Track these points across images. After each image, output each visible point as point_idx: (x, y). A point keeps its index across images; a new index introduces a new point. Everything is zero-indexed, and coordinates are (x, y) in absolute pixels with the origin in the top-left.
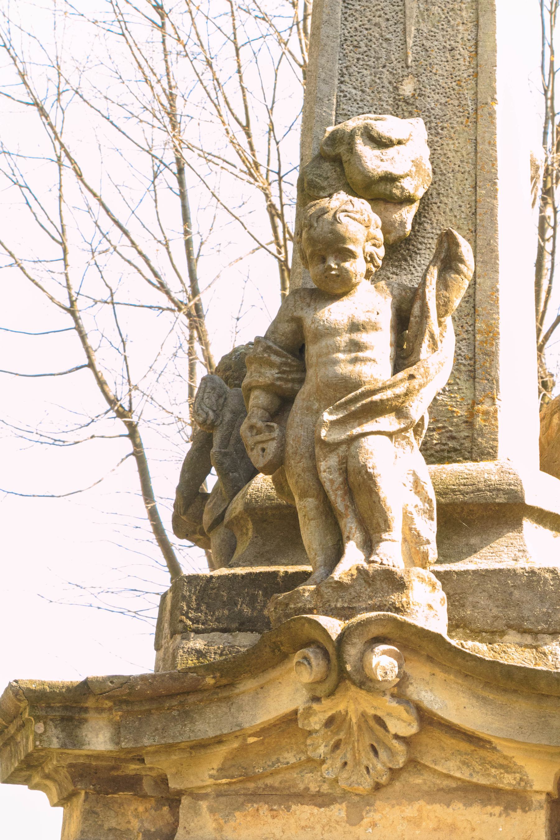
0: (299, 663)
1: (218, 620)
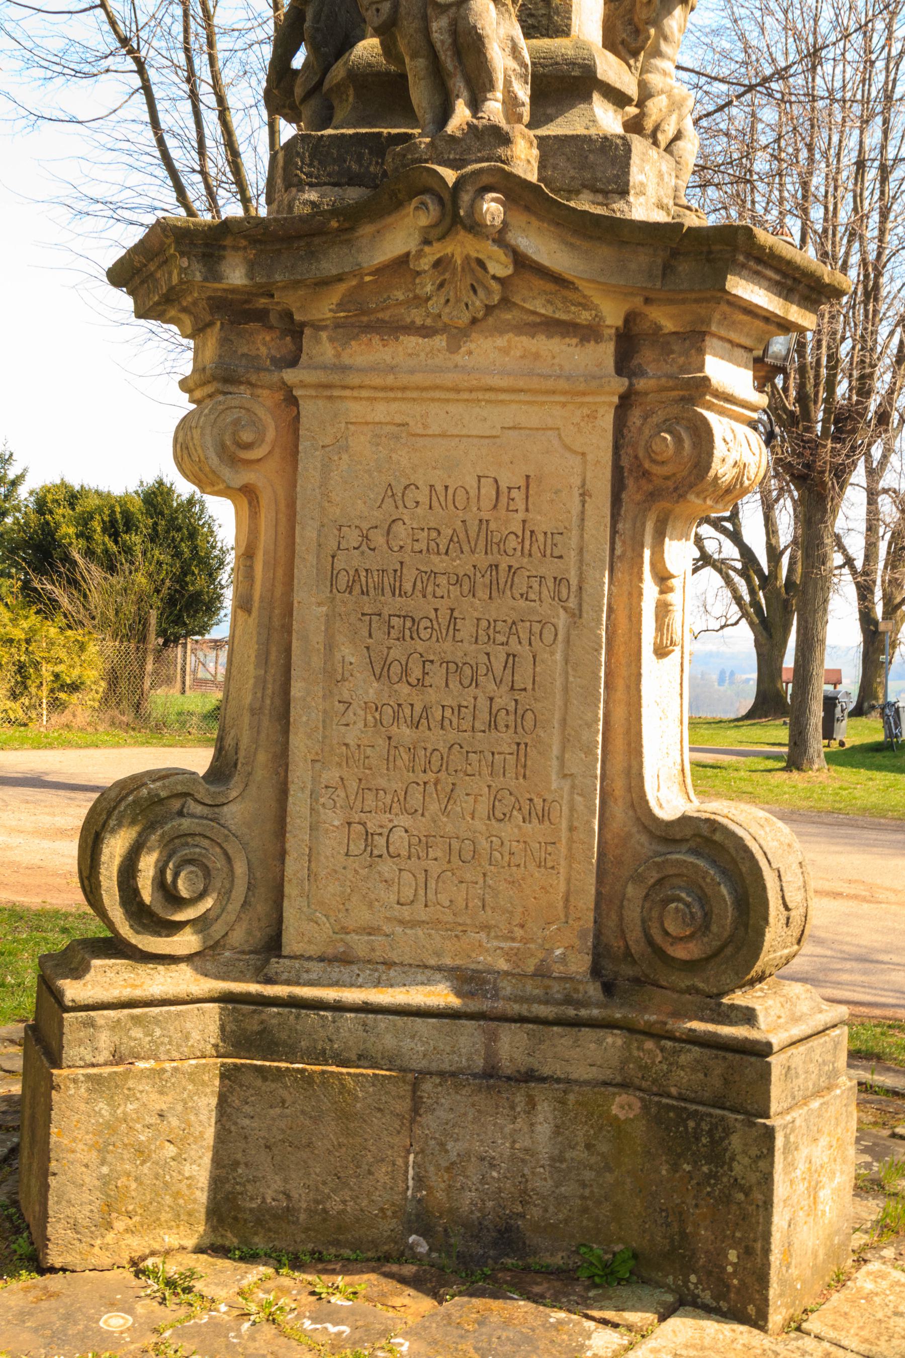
0: (417, 208)
1: (329, 175)
